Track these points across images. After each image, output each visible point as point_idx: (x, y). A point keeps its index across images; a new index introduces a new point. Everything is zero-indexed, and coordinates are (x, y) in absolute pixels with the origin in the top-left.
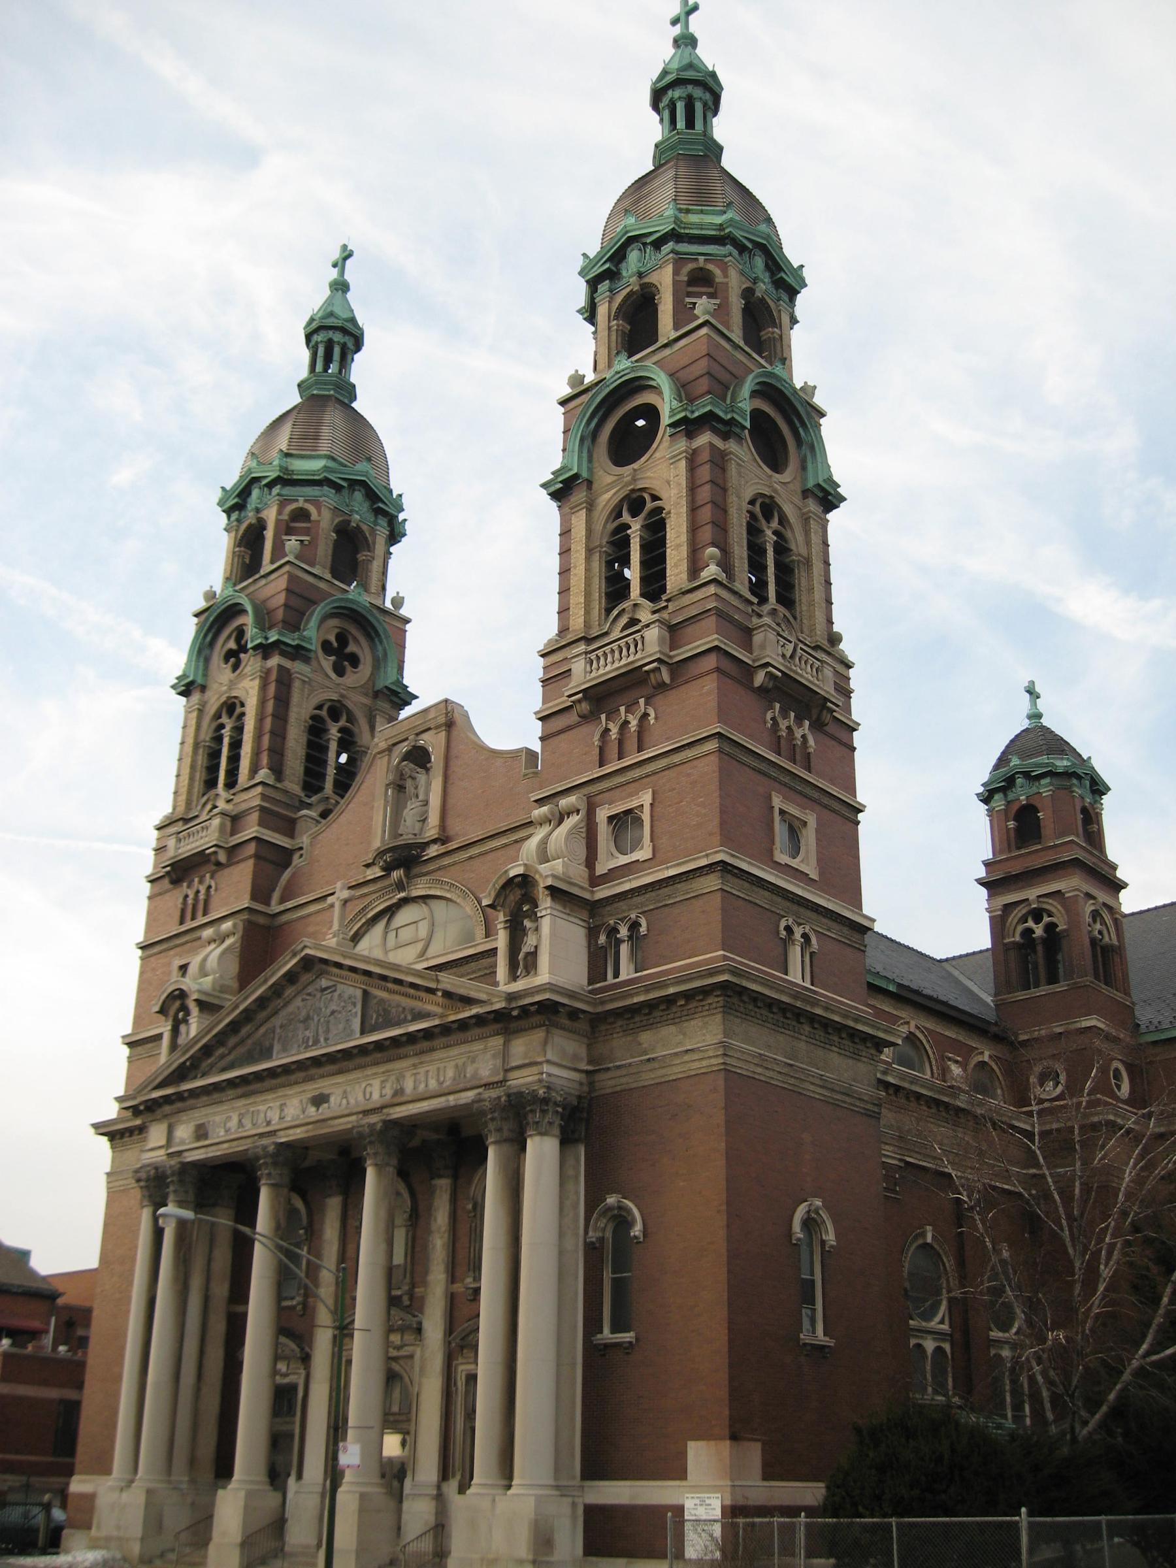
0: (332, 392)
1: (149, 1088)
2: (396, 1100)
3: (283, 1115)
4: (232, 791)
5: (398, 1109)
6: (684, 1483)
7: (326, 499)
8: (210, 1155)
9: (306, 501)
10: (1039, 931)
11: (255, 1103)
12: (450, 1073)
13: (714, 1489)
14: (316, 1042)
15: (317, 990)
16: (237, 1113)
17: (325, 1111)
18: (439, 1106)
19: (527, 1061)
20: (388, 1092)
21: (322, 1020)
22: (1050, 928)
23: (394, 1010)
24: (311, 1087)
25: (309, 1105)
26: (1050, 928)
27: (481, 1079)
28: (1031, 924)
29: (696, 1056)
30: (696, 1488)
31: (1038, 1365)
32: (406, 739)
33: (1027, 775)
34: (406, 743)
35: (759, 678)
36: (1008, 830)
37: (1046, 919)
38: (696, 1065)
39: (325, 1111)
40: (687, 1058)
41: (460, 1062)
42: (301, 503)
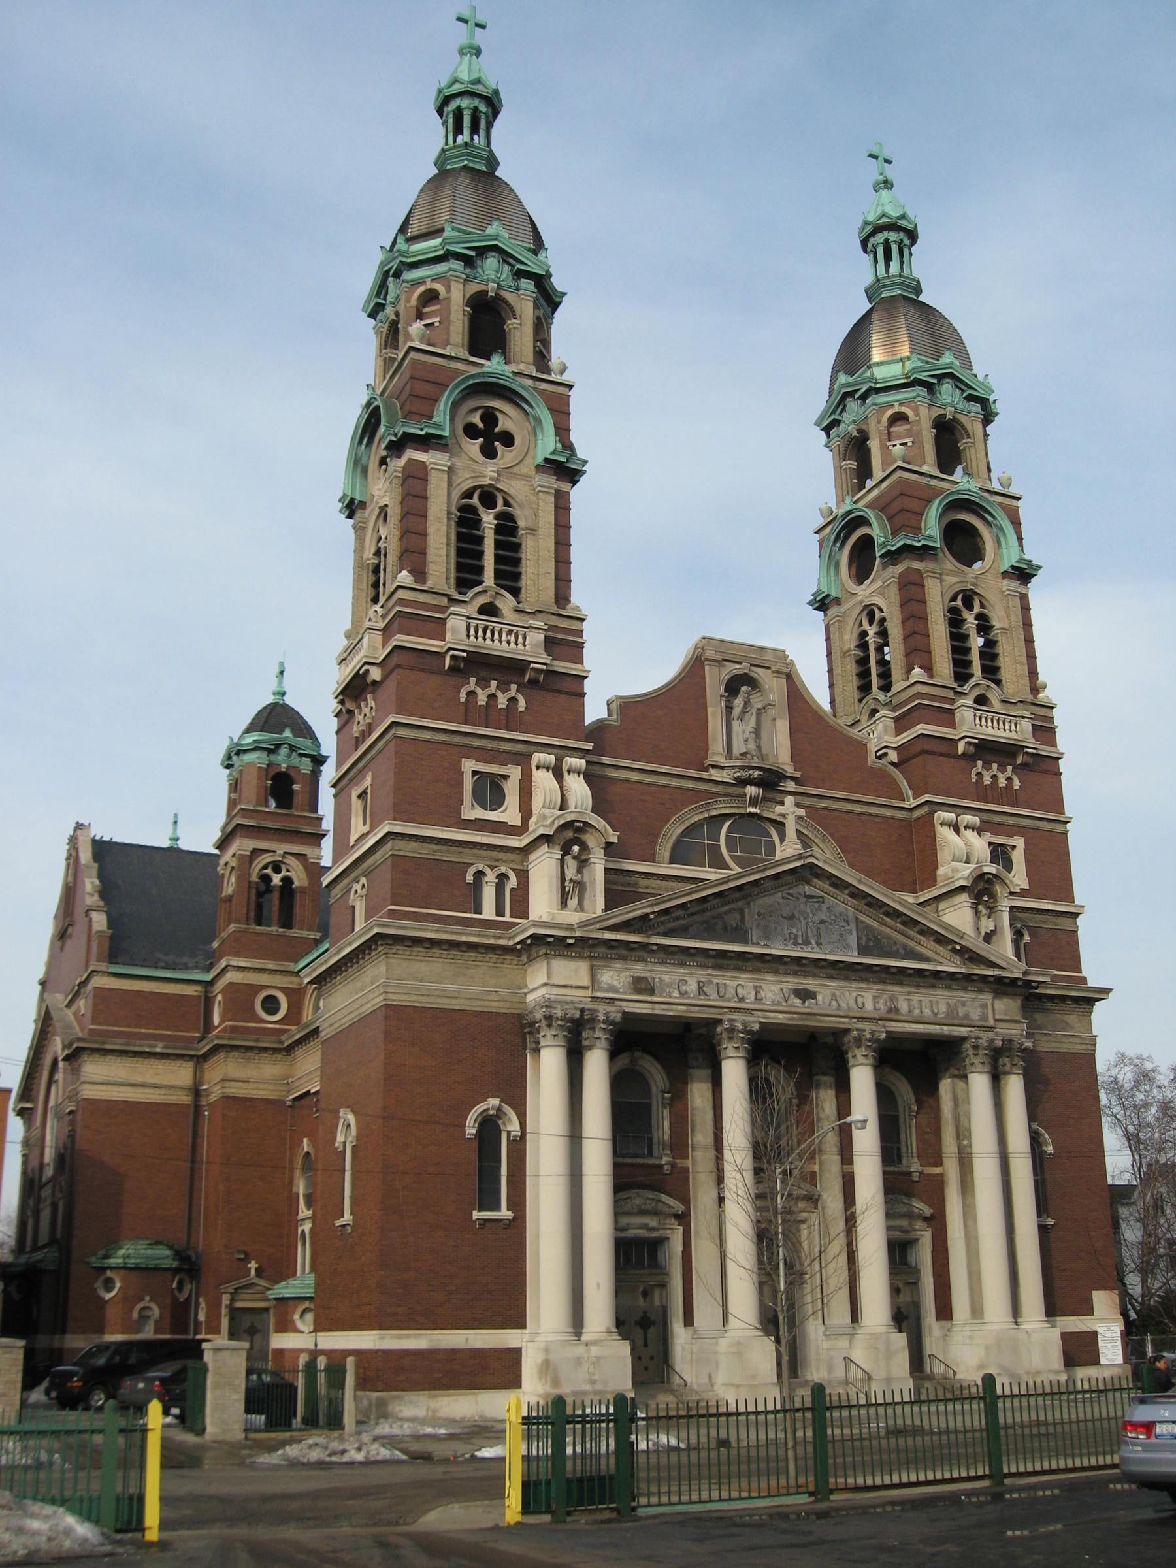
0: (899, 292)
1: (598, 926)
2: (890, 1016)
3: (759, 997)
4: (889, 694)
5: (893, 1024)
6: (1093, 1317)
7: (452, 273)
8: (657, 1012)
9: (900, 405)
10: (276, 879)
11: (723, 976)
12: (943, 1009)
13: (1115, 1320)
14: (806, 942)
15: (800, 894)
16: (695, 980)
17: (810, 1006)
18: (933, 1032)
19: (1007, 1018)
20: (881, 1005)
21: (811, 924)
22: (287, 881)
23: (884, 940)
24: (796, 981)
25: (792, 996)
26: (287, 881)
27: (972, 1020)
28: (269, 871)
29: (1078, 1041)
30: (1103, 1320)
31: (309, 1210)
32: (740, 663)
33: (292, 748)
34: (738, 666)
35: (961, 747)
36: (266, 787)
37: (284, 873)
38: (1078, 1046)
39: (810, 1006)
40: (1071, 1040)
41: (952, 1002)
42: (897, 408)
